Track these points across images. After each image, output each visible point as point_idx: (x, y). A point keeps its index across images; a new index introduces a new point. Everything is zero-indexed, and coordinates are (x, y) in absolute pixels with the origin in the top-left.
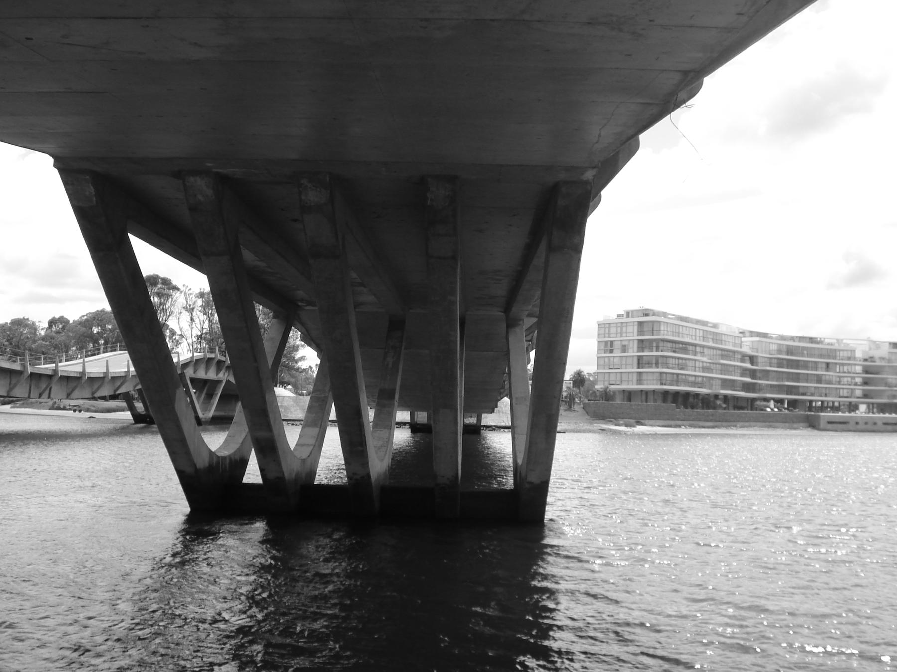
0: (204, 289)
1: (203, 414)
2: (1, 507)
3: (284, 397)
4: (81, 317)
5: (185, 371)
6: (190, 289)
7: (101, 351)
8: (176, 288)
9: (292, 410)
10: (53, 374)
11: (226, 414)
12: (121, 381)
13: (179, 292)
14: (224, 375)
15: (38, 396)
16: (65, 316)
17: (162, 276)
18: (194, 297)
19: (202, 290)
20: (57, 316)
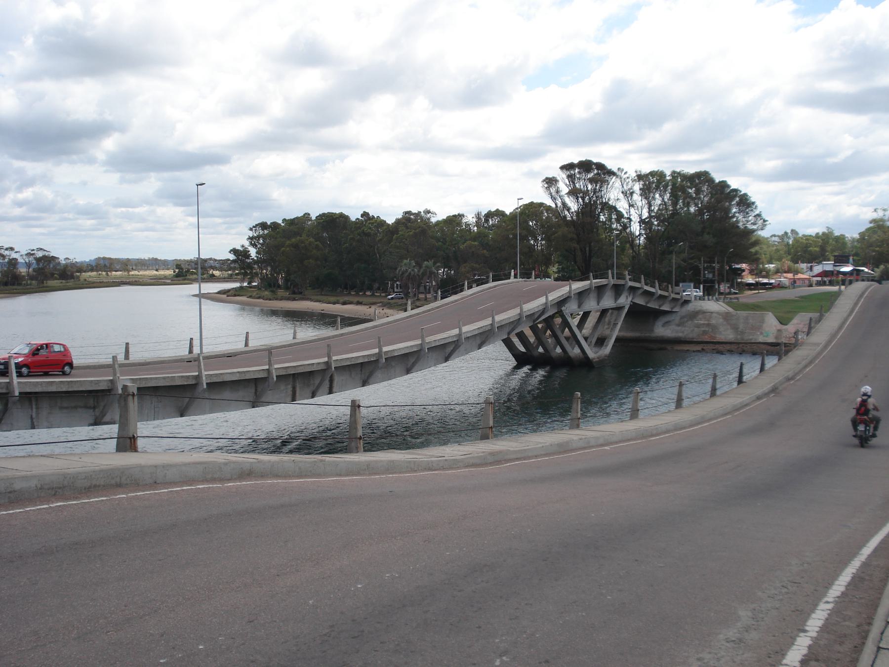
0: (640, 171)
1: (596, 353)
2: (76, 666)
3: (712, 313)
4: (514, 210)
5: (563, 308)
6: (626, 173)
7: (466, 287)
8: (611, 173)
9: (722, 329)
10: (325, 368)
11: (643, 335)
12: (453, 346)
13: (614, 177)
14: (627, 298)
15: (311, 395)
16: (500, 209)
17: (595, 161)
18: (631, 182)
19: (639, 173)
20: (493, 210)
